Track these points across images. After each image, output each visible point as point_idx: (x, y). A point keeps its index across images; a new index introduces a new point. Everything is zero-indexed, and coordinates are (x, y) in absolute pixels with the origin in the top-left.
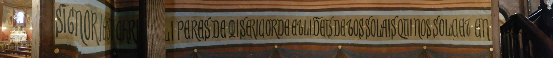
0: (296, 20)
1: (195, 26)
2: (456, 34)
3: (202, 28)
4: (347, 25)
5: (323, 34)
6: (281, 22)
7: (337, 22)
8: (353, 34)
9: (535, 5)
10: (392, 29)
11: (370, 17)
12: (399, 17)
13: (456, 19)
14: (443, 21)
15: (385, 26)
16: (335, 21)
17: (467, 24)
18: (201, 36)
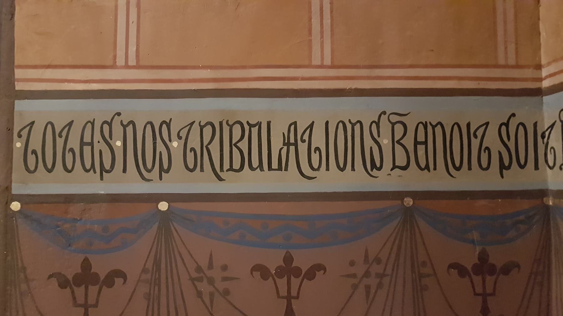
1: (25, 127)
2: (90, 163)
4: (60, 136)
6: (438, 129)
7: (130, 129)
15: (292, 140)
16: (125, 127)
17: (184, 138)
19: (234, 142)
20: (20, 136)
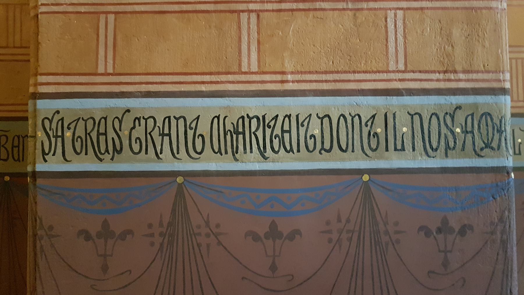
1: (304, 121)
5: (16, 158)
9: (296, 70)
11: (54, 114)
12: (61, 112)
15: (166, 131)
16: (322, 119)
18: (103, 151)
19: (88, 132)
20: (367, 126)
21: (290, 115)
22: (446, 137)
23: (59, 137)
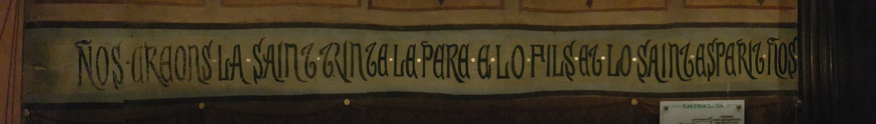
0: (587, 47)
2: (441, 71)
3: (702, 59)
4: (303, 53)
8: (377, 73)
10: (708, 65)
13: (170, 46)
14: (183, 49)
16: (424, 47)
20: (303, 53)
21: (415, 45)
22: (708, 65)
23: (237, 65)
